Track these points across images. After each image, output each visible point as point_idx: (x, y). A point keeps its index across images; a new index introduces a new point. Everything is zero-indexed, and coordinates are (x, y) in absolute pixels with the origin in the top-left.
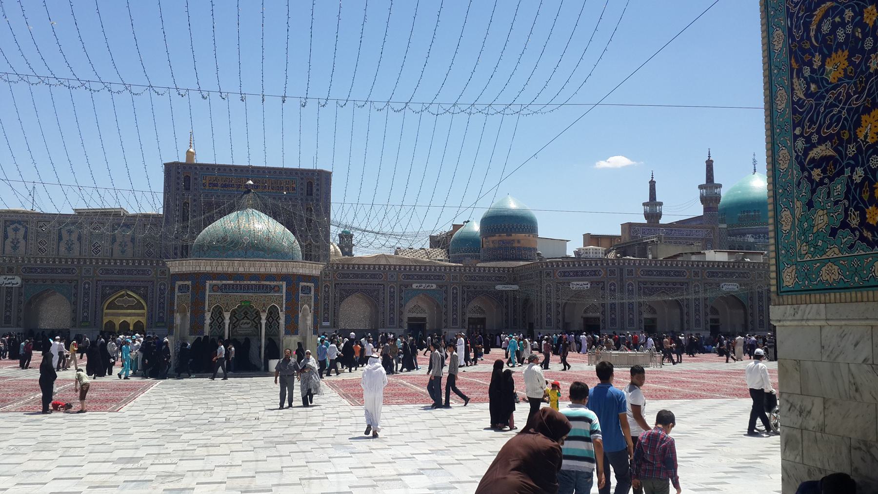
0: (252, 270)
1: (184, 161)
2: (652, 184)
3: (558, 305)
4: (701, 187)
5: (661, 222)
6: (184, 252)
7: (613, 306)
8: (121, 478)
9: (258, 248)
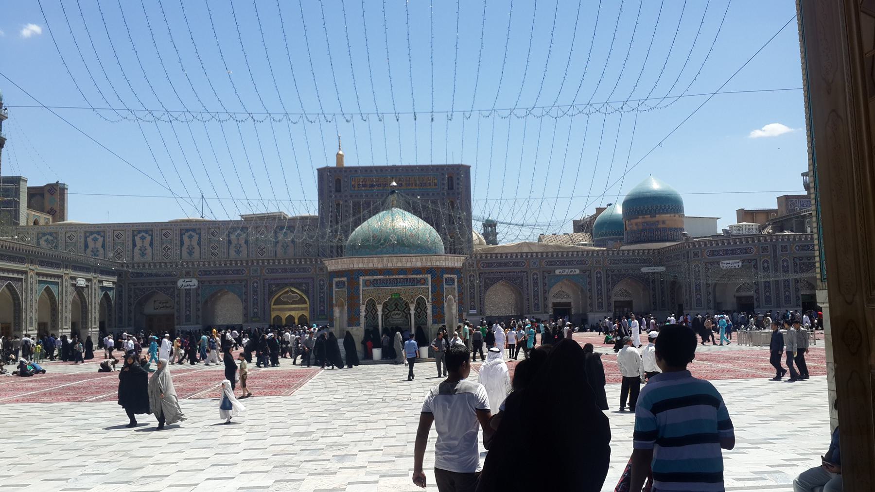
0: (400, 265)
6: (339, 251)
7: (767, 285)
8: (299, 448)
9: (404, 244)
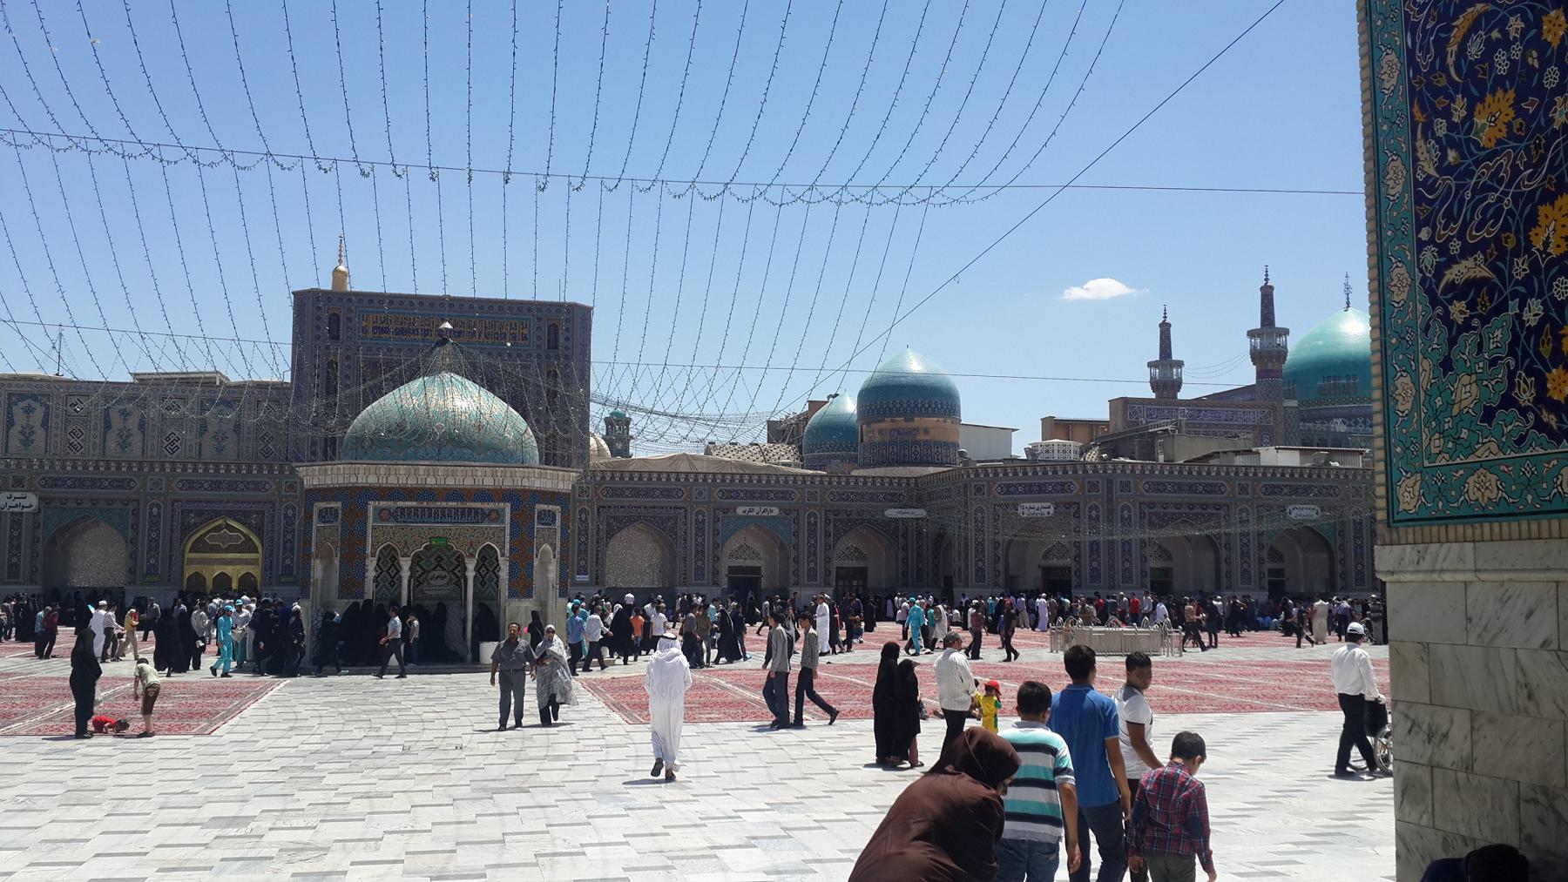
0: (450, 482)
1: (329, 288)
2: (1165, 329)
3: (996, 545)
4: (1251, 334)
5: (1181, 396)
6: (329, 450)
7: (1094, 546)
8: (217, 854)
9: (461, 443)
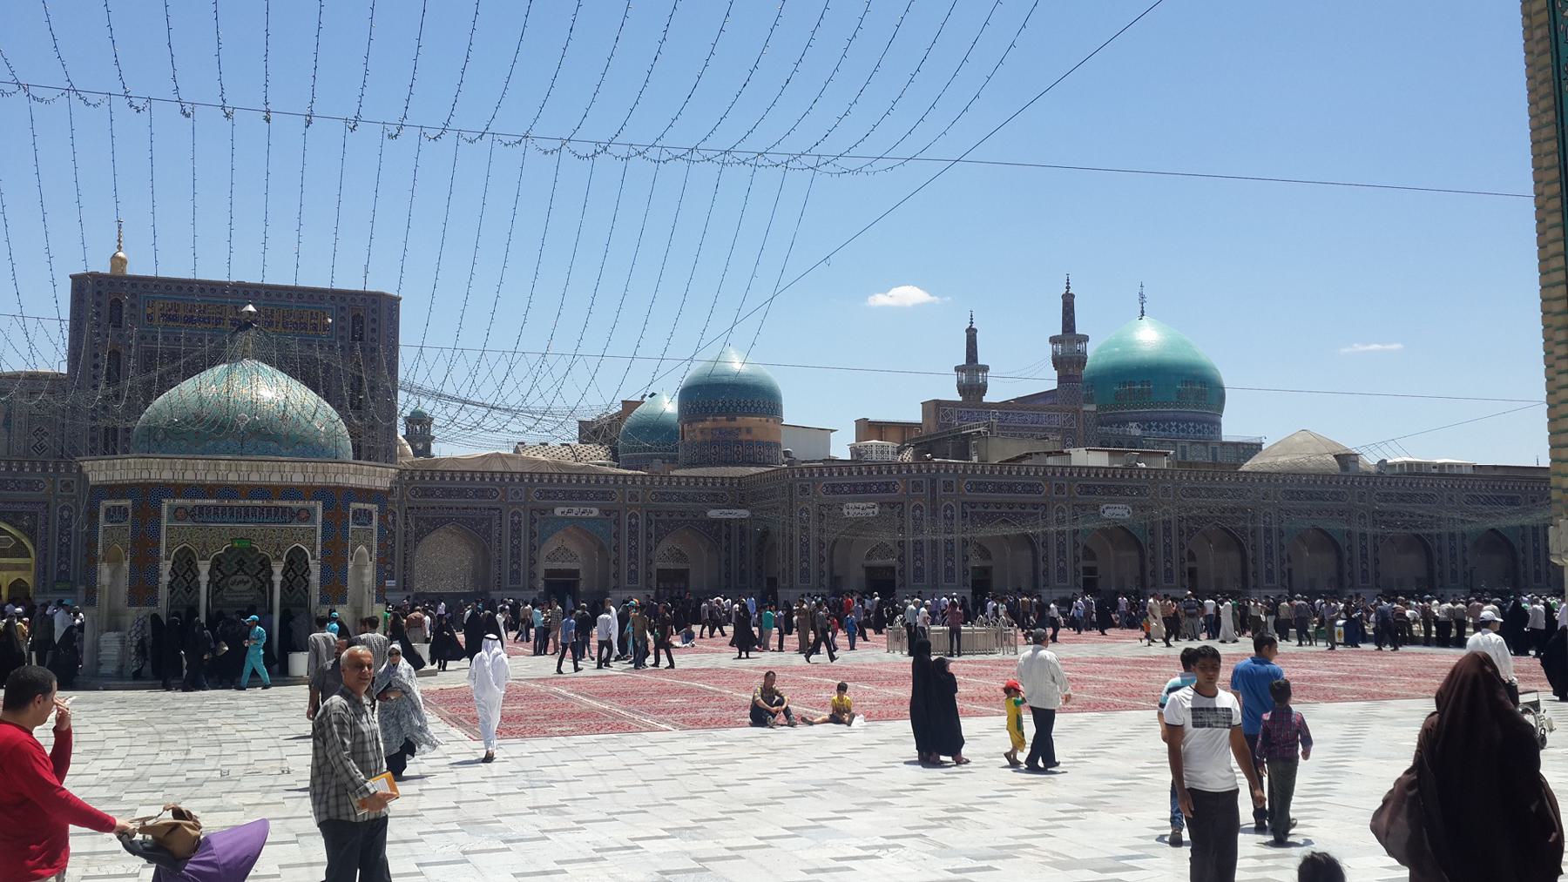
0: (255, 478)
1: (107, 271)
2: (971, 334)
3: (821, 545)
4: (1053, 340)
5: (986, 399)
6: (112, 442)
9: (266, 436)
